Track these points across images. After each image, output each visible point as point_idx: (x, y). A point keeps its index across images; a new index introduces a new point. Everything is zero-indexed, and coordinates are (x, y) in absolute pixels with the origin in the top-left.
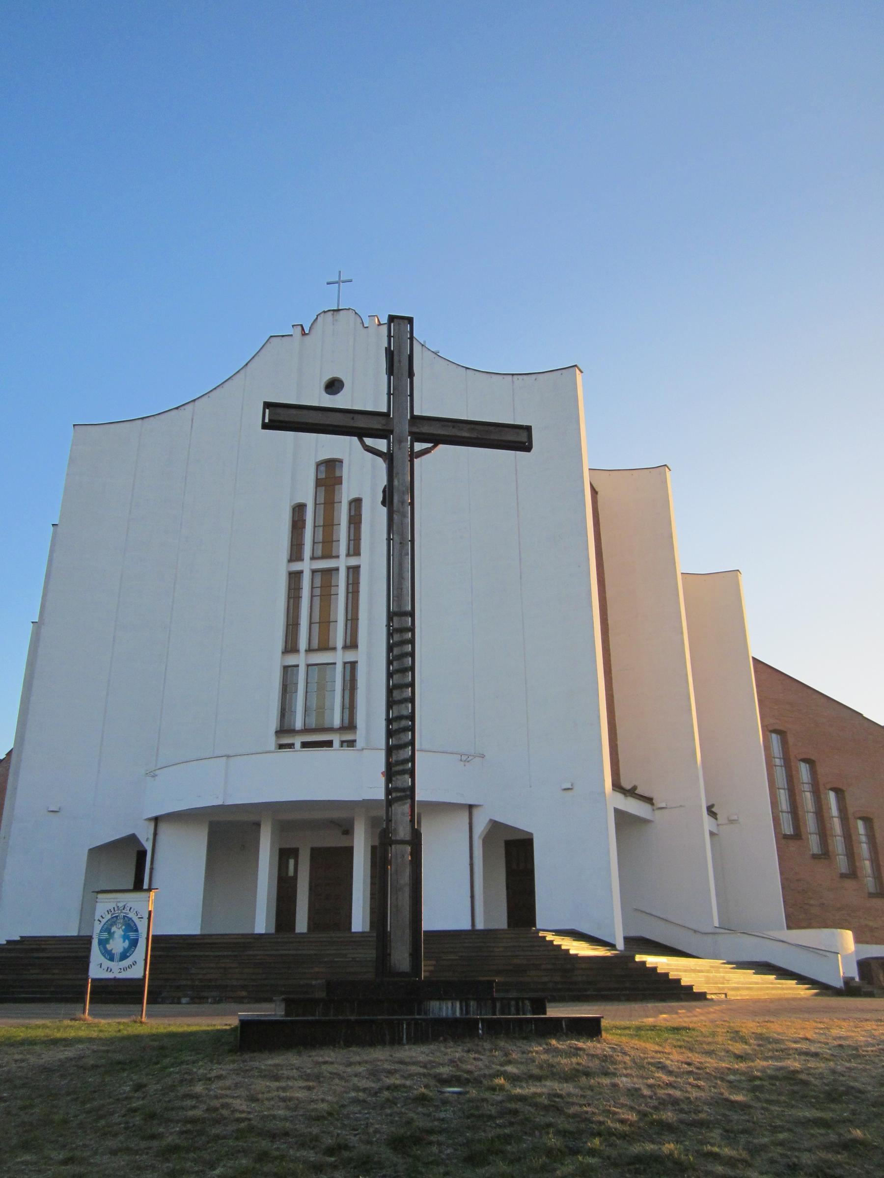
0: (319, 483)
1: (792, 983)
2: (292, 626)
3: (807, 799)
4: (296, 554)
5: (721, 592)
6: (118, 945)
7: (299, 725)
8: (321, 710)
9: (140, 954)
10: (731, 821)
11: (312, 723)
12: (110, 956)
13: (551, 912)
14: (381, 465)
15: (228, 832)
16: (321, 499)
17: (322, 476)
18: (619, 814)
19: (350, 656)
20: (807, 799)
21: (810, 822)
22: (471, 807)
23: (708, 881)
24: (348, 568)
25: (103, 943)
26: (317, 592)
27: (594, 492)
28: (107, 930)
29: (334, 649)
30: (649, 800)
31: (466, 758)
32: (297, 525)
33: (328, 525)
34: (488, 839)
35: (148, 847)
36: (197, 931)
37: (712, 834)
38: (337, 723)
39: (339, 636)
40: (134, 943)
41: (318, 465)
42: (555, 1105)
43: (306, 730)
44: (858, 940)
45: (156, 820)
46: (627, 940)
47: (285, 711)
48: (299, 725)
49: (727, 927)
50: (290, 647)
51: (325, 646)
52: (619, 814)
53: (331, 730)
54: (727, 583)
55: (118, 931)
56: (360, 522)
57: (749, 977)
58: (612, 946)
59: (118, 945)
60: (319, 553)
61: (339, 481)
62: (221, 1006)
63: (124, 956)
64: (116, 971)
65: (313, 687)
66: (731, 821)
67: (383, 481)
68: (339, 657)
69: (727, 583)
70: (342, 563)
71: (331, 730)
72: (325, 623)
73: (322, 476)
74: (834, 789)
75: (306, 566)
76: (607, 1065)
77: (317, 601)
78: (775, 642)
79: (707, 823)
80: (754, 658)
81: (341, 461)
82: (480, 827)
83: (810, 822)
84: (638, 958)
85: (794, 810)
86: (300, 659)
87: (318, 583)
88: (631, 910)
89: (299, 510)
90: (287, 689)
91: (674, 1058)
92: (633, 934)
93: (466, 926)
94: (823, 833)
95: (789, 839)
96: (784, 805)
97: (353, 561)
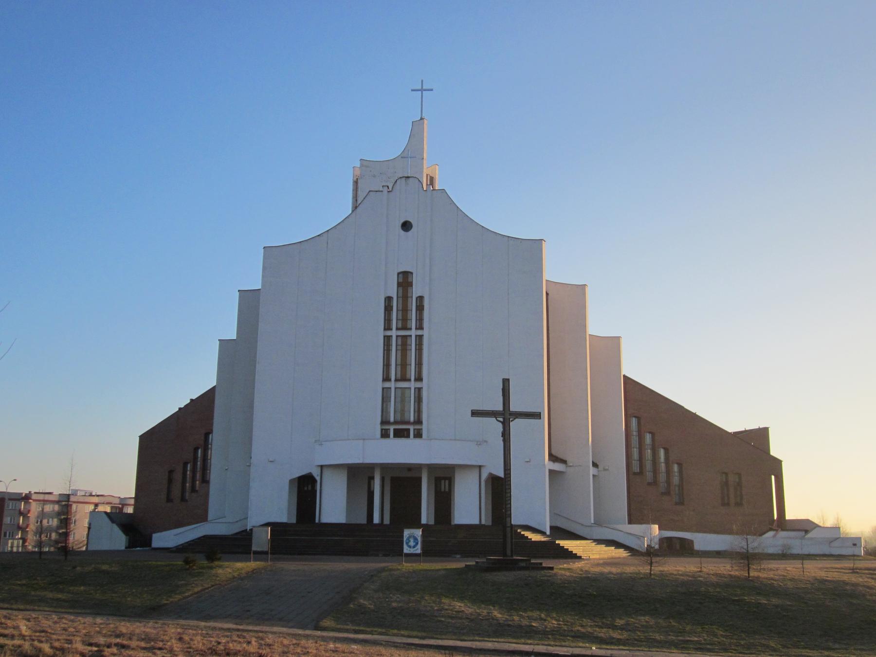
0: (399, 285)
1: (621, 550)
2: (387, 365)
3: (649, 453)
4: (388, 327)
5: (611, 347)
6: (412, 543)
7: (392, 420)
8: (403, 411)
9: (419, 546)
10: (605, 470)
11: (399, 419)
12: (410, 547)
13: (518, 516)
14: (501, 425)
15: (358, 475)
16: (400, 294)
17: (401, 280)
18: (551, 472)
19: (418, 385)
20: (649, 453)
21: (648, 465)
22: (480, 467)
23: (589, 502)
24: (416, 336)
25: (407, 543)
26: (399, 347)
27: (547, 294)
28: (408, 539)
29: (410, 380)
30: (564, 462)
31: (479, 443)
32: (388, 309)
33: (405, 310)
34: (486, 481)
35: (318, 478)
36: (344, 521)
37: (594, 476)
38: (412, 419)
39: (412, 372)
40: (417, 544)
41: (398, 274)
42: (548, 580)
43: (396, 423)
44: (660, 529)
45: (322, 467)
46: (552, 528)
47: (384, 411)
48: (392, 420)
49: (598, 523)
50: (386, 379)
51: (404, 378)
52: (551, 472)
53: (408, 423)
54: (615, 342)
55: (412, 540)
56: (423, 309)
57: (603, 547)
58: (543, 533)
59: (412, 543)
60: (400, 326)
61: (411, 284)
62: (387, 558)
63: (414, 547)
64: (412, 551)
65: (399, 399)
66: (605, 470)
67: (502, 430)
68: (413, 385)
69: (615, 342)
70: (413, 333)
71: (408, 423)
72: (404, 365)
73: (401, 280)
74: (664, 448)
75: (394, 333)
76: (555, 574)
77: (399, 353)
78: (637, 366)
79: (592, 471)
81: (412, 273)
82: (484, 476)
83: (648, 465)
84: (557, 542)
85: (641, 459)
86: (392, 385)
87: (400, 343)
88: (554, 514)
89: (389, 299)
90: (385, 399)
91: (568, 574)
92: (554, 524)
93: (477, 522)
94: (655, 471)
95: (633, 475)
96: (636, 455)
97: (419, 332)
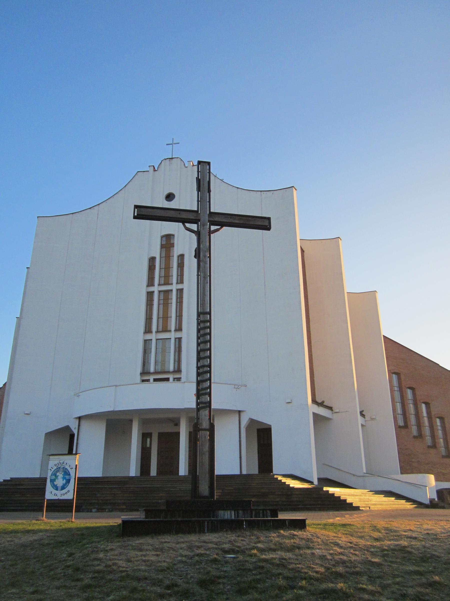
0: (162, 246)
1: (403, 501)
2: (149, 319)
3: (411, 408)
4: (151, 283)
5: (367, 302)
6: (60, 482)
7: (152, 370)
8: (163, 362)
9: (71, 486)
10: (372, 419)
11: (159, 369)
12: (56, 488)
13: (280, 465)
14: (194, 237)
15: (116, 425)
16: (163, 255)
17: (164, 243)
18: (315, 415)
19: (178, 335)
20: (411, 408)
21: (412, 420)
22: (240, 412)
23: (360, 450)
24: (177, 290)
25: (52, 481)
26: (162, 302)
27: (302, 251)
28: (55, 474)
29: (170, 331)
30: (330, 408)
31: (237, 387)
32: (151, 268)
33: (167, 268)
34: (248, 428)
35: (76, 432)
36: (100, 475)
37: (362, 425)
38: (172, 369)
39: (173, 324)
40: (68, 481)
41: (162, 237)
42: (283, 564)
43: (156, 373)
44: (437, 480)
45: (80, 418)
46: (319, 480)
47: (145, 363)
48: (152, 370)
49: (370, 473)
50: (148, 330)
51: (166, 330)
52: (315, 415)
53: (168, 372)
54: (370, 298)
55: (60, 475)
56: (183, 266)
57: (381, 498)
58: (312, 483)
59: (60, 482)
60: (162, 282)
61: (173, 245)
62: (112, 513)
63: (63, 488)
64: (59, 495)
65: (160, 350)
66: (372, 419)
67: (195, 246)
68: (173, 335)
69: (370, 298)
70: (174, 287)
71: (168, 372)
72: (165, 318)
73: (164, 243)
74: (424, 403)
75: (156, 289)
76: (309, 543)
77: (161, 306)
78: (395, 327)
79: (360, 420)
80: (384, 336)
81: (173, 235)
82: (244, 422)
83: (412, 420)
84: (325, 489)
85: (404, 413)
86: (153, 336)
87: (162, 297)
88: (321, 464)
89: (152, 260)
90: (146, 351)
91: (343, 540)
92: (322, 476)
93: (237, 472)
94: (419, 425)
95: (402, 428)
96: (399, 410)
97: (180, 286)
